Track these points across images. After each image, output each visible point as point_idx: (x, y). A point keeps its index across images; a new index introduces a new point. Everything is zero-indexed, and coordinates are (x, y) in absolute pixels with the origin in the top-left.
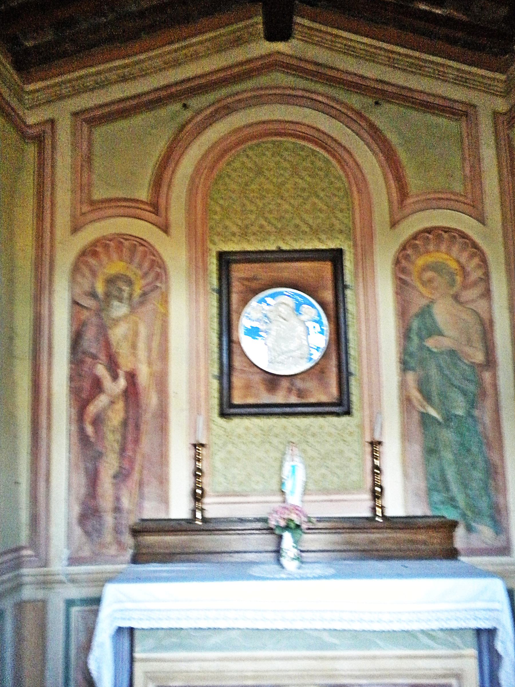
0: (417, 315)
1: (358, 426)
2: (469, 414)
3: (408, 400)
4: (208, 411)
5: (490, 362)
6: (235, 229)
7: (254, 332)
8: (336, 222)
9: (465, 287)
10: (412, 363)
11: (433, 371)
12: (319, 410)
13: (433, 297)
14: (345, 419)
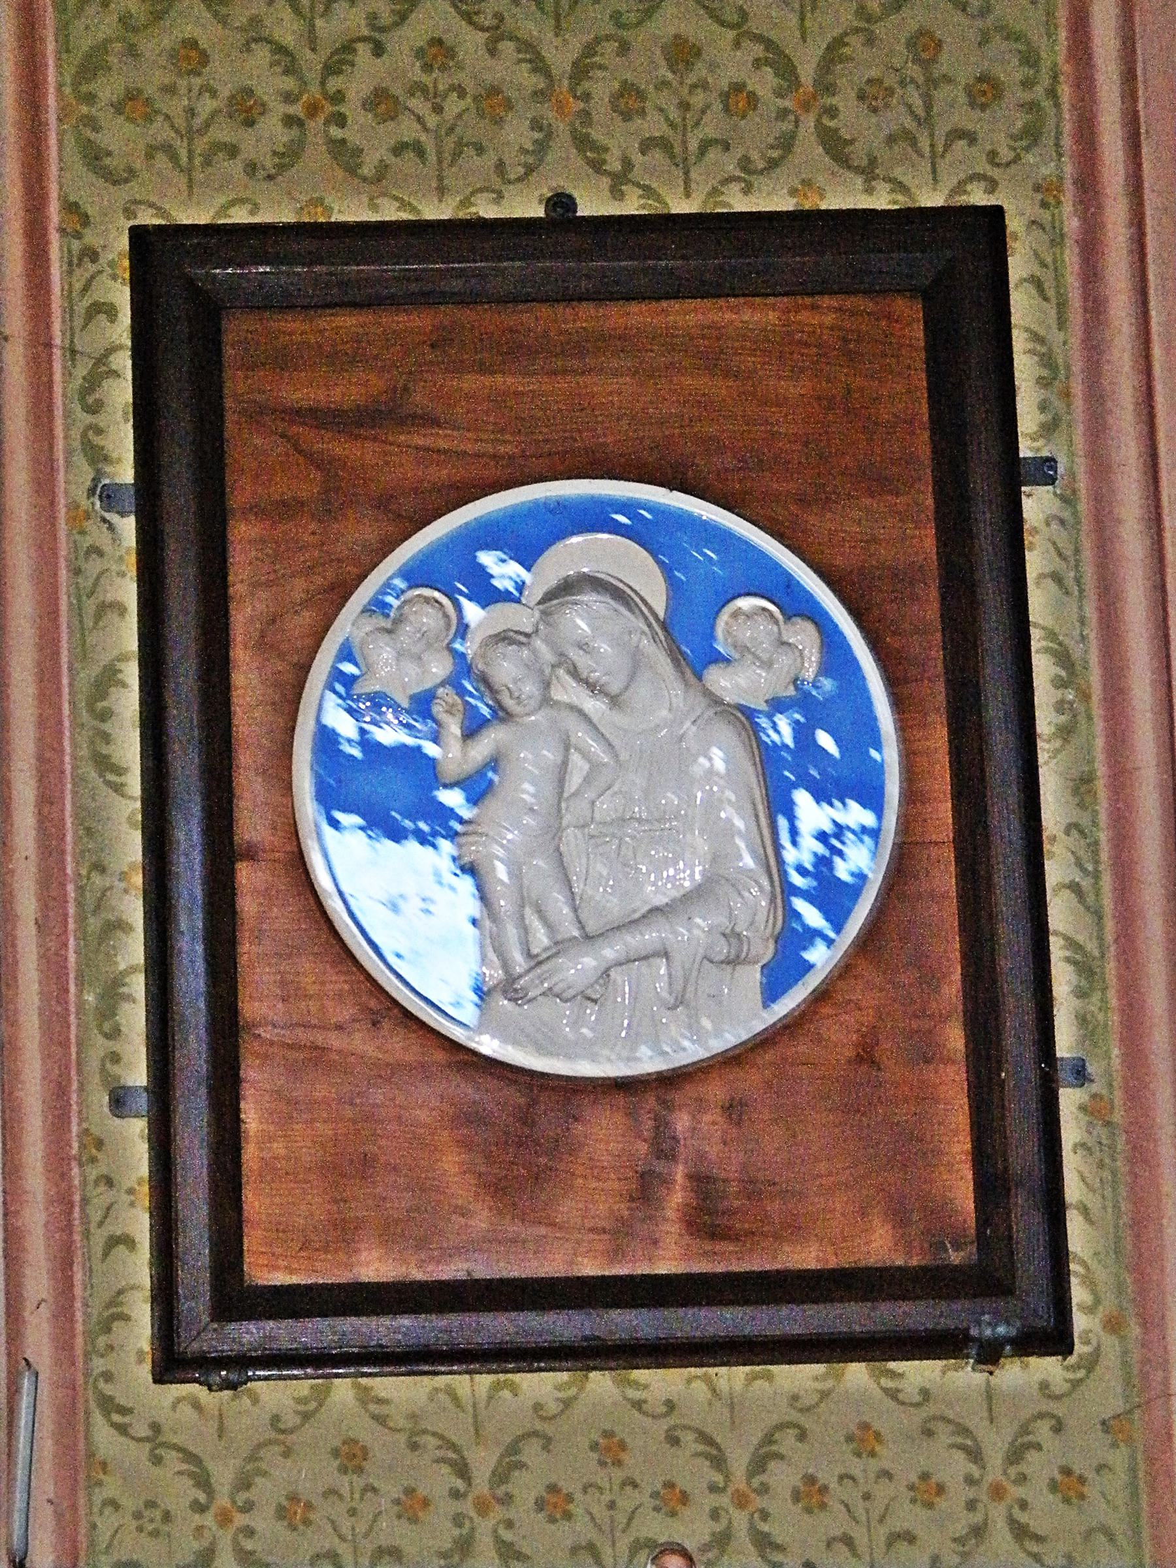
4: (83, 1330)
6: (260, 74)
7: (397, 798)
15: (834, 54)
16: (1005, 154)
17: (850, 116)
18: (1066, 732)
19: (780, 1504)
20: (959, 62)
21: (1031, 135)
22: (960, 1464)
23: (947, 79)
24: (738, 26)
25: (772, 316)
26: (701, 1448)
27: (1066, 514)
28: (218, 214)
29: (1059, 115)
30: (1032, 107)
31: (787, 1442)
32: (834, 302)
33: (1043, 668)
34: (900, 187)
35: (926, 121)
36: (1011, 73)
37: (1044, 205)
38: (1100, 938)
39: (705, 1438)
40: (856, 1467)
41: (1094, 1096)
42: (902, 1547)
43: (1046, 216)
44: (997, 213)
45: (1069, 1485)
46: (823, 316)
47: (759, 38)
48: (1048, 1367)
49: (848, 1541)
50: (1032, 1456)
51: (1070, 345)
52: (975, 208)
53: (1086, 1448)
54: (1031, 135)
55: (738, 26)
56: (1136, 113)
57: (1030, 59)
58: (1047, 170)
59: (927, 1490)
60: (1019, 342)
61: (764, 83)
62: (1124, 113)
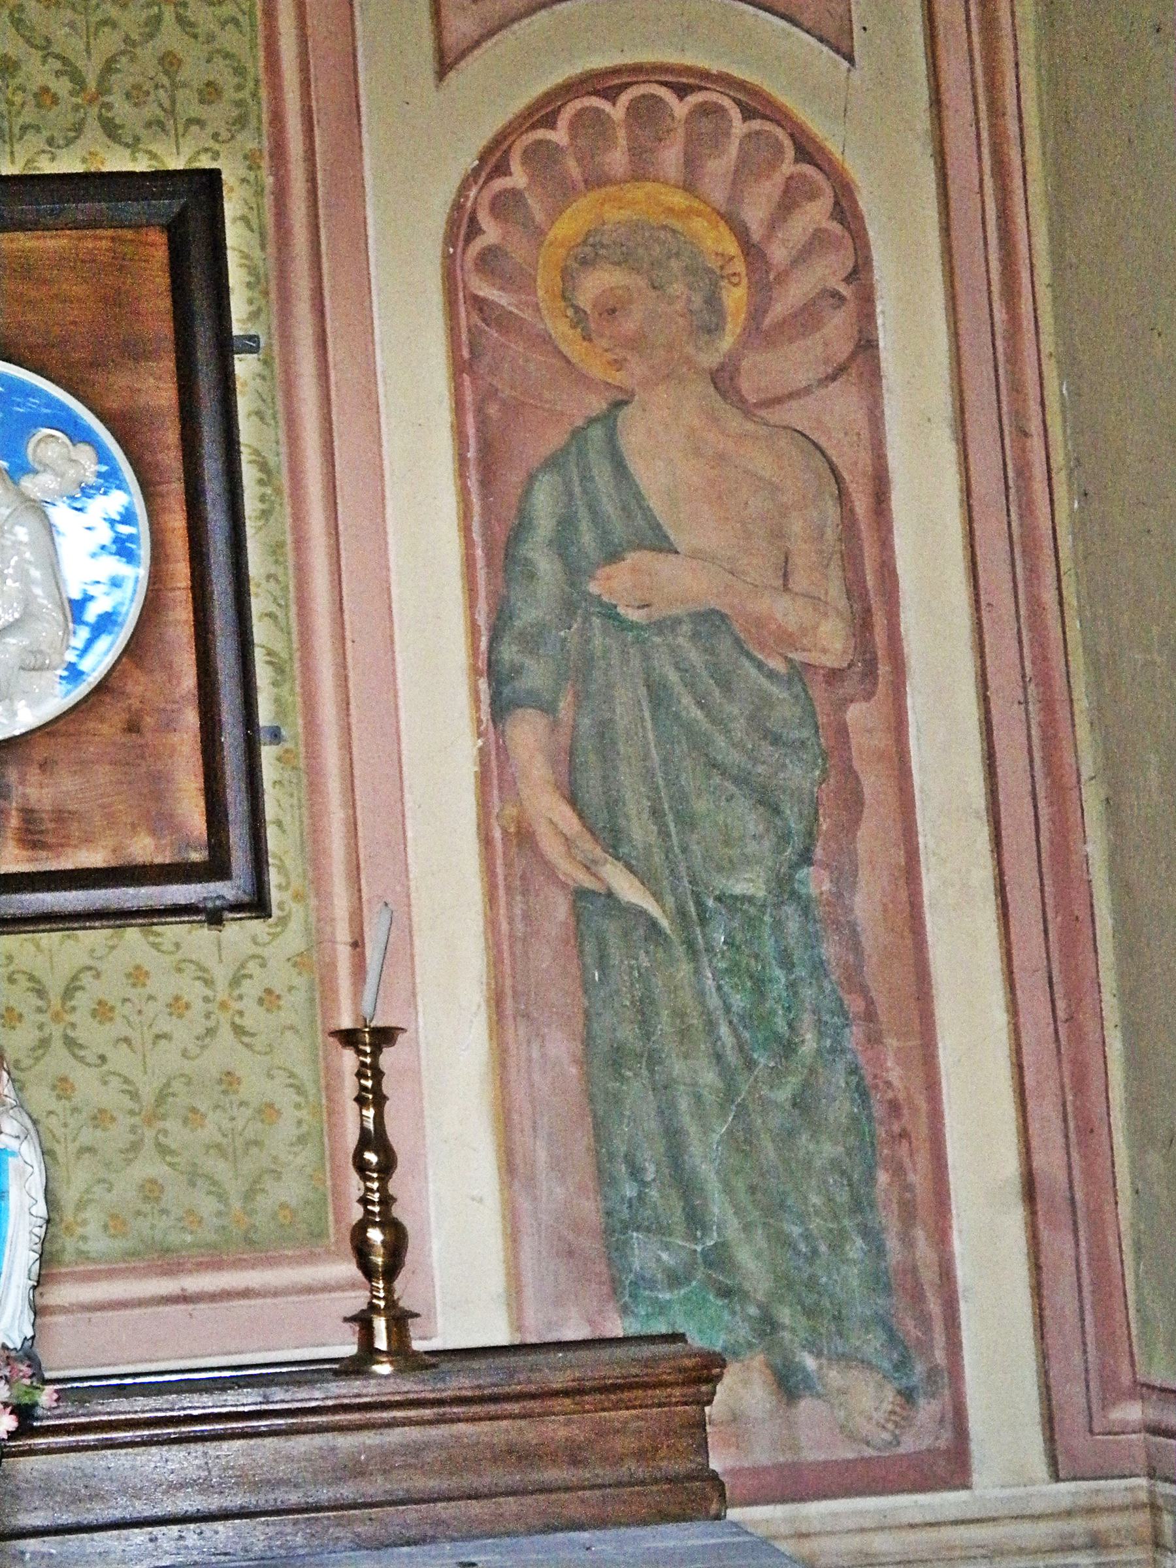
0: (553, 463)
1: (298, 962)
2: (784, 887)
3: (523, 837)
5: (876, 658)
8: (191, 53)
9: (759, 333)
10: (536, 675)
11: (627, 704)
12: (114, 897)
13: (617, 378)
14: (240, 932)
15: (109, 68)
16: (224, 135)
17: (122, 109)
18: (265, 514)
19: (81, 1017)
20: (193, 72)
21: (241, 121)
22: (199, 988)
23: (185, 85)
24: (44, 48)
25: (64, 242)
26: (31, 985)
27: (266, 373)
28: (190, 160)
29: (260, 109)
30: (239, 104)
31: (86, 979)
32: (110, 232)
33: (249, 474)
34: (153, 156)
35: (172, 112)
36: (227, 81)
37: (250, 168)
38: (290, 648)
39: (32, 978)
40: (131, 993)
41: (287, 751)
42: (163, 1042)
43: (251, 176)
44: (214, 176)
45: (269, 999)
46: (99, 242)
47: (57, 57)
48: (256, 926)
49: (126, 1040)
50: (246, 983)
51: (266, 262)
52: (204, 170)
53: (280, 975)
54: (241, 121)
55: (44, 48)
56: (310, 107)
57: (240, 71)
58: (252, 145)
59: (177, 1006)
60: (233, 260)
61: (62, 87)
62: (302, 108)
